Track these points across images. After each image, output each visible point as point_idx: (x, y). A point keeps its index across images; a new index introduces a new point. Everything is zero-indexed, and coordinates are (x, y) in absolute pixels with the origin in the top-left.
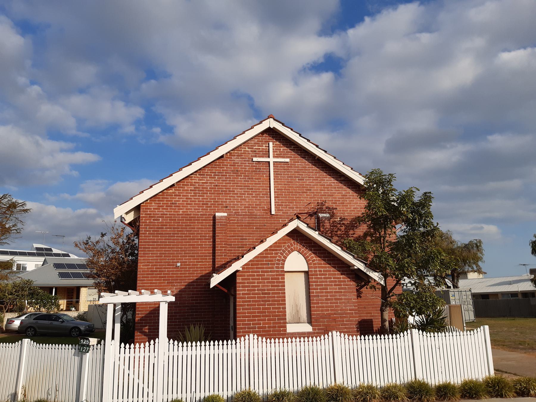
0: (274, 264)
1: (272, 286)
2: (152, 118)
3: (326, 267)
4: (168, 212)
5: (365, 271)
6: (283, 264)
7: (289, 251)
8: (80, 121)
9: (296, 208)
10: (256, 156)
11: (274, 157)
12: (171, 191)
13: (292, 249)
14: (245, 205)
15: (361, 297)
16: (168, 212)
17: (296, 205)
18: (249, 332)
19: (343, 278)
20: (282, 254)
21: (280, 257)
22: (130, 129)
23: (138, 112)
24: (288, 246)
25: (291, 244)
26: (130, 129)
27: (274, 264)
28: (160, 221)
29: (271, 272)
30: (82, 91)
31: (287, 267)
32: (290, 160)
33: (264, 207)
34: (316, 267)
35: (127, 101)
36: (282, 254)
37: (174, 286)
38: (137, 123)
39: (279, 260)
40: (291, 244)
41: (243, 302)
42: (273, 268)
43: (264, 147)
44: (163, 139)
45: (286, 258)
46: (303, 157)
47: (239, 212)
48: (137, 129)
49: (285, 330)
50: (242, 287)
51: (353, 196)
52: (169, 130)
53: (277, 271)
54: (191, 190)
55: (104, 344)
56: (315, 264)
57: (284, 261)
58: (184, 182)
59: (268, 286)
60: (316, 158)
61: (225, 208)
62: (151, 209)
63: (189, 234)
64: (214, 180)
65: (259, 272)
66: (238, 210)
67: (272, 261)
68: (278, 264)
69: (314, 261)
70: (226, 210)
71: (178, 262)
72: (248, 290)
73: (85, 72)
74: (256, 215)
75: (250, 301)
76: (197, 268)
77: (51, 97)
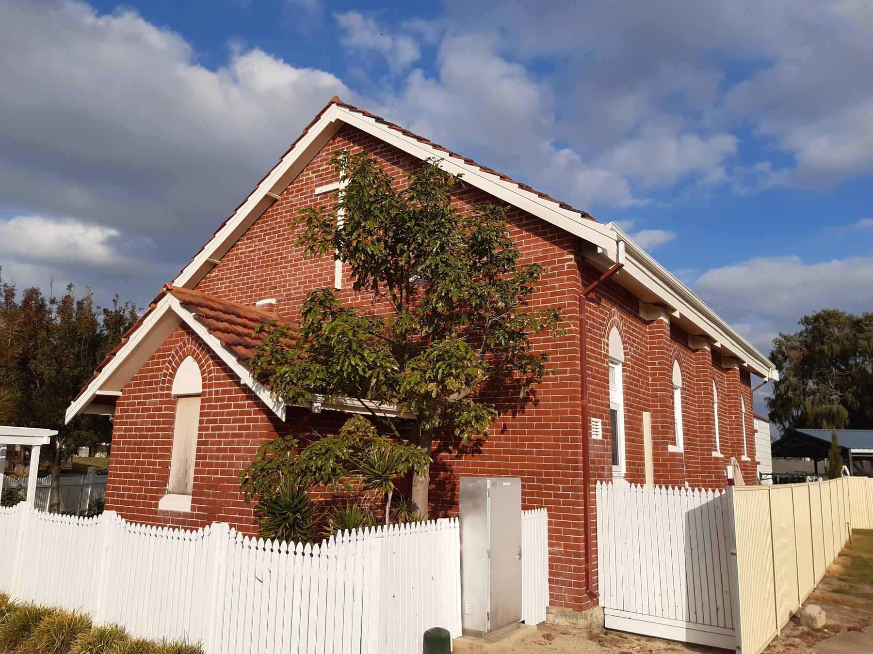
2: (752, 149)
3: (224, 385)
5: (253, 389)
6: (171, 382)
8: (635, 185)
12: (214, 274)
15: (480, 452)
19: (249, 406)
21: (167, 369)
22: (718, 175)
23: (727, 143)
26: (718, 175)
27: (157, 383)
30: (632, 134)
31: (177, 389)
35: (704, 133)
38: (728, 162)
39: (165, 375)
44: (779, 179)
45: (175, 370)
46: (394, 164)
47: (291, 294)
48: (729, 172)
49: (156, 505)
52: (785, 160)
58: (229, 256)
73: (626, 108)
77: (589, 158)
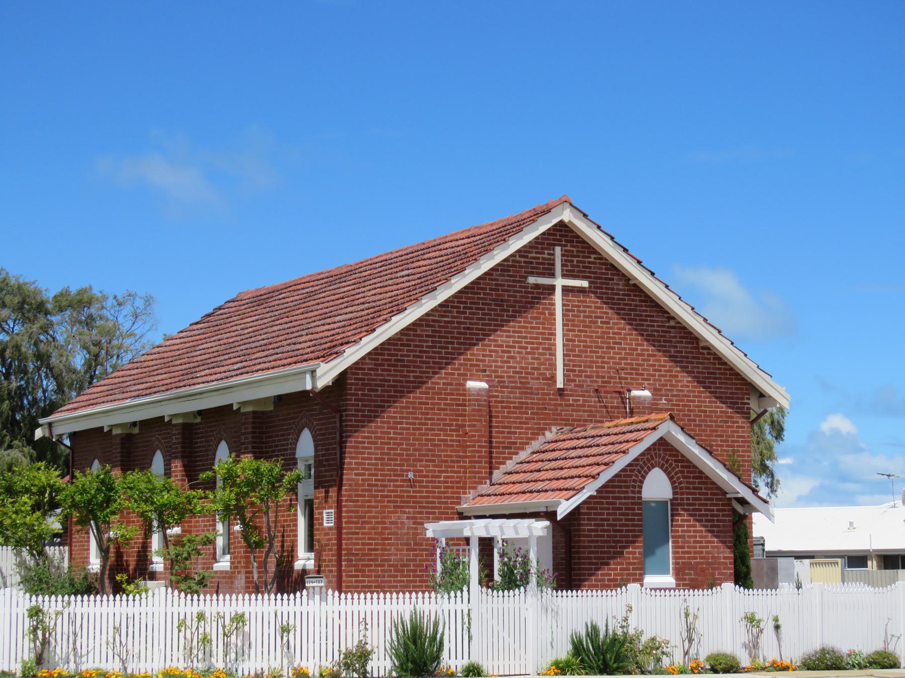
0: (628, 487)
1: (626, 520)
4: (392, 375)
7: (652, 464)
9: (598, 377)
10: (532, 274)
11: (564, 276)
13: (652, 464)
14: (515, 368)
16: (392, 375)
17: (597, 372)
18: (628, 581)
20: (642, 468)
21: (637, 476)
24: (648, 459)
25: (652, 456)
27: (628, 487)
28: (379, 393)
29: (625, 498)
32: (590, 283)
33: (545, 374)
34: (682, 494)
36: (639, 472)
37: (405, 513)
39: (634, 481)
40: (652, 456)
41: (589, 542)
42: (627, 492)
43: (546, 256)
45: (644, 477)
47: (504, 382)
50: (588, 519)
51: (637, 340)
53: (633, 498)
54: (427, 336)
55: (468, 591)
56: (682, 488)
57: (642, 482)
59: (621, 520)
60: (631, 282)
61: (481, 373)
62: (364, 369)
63: (426, 419)
64: (465, 318)
65: (427, 492)
66: (503, 377)
67: (626, 481)
68: (634, 487)
69: (680, 483)
70: (484, 376)
71: (409, 470)
72: (595, 525)
74: (532, 388)
75: (597, 541)
76: (439, 482)
